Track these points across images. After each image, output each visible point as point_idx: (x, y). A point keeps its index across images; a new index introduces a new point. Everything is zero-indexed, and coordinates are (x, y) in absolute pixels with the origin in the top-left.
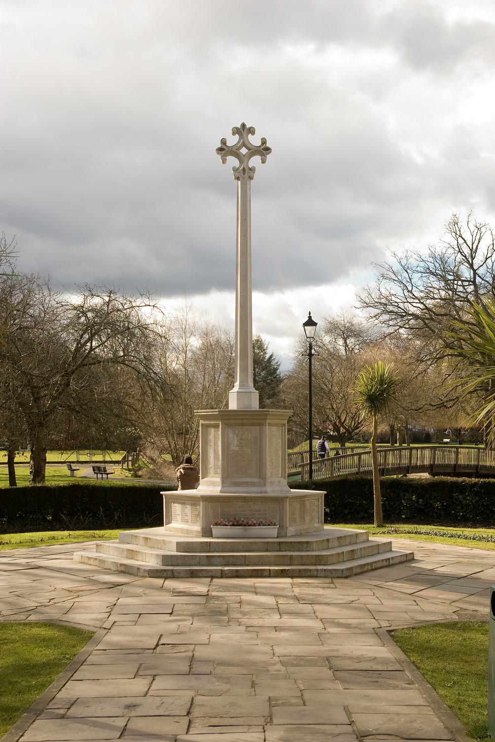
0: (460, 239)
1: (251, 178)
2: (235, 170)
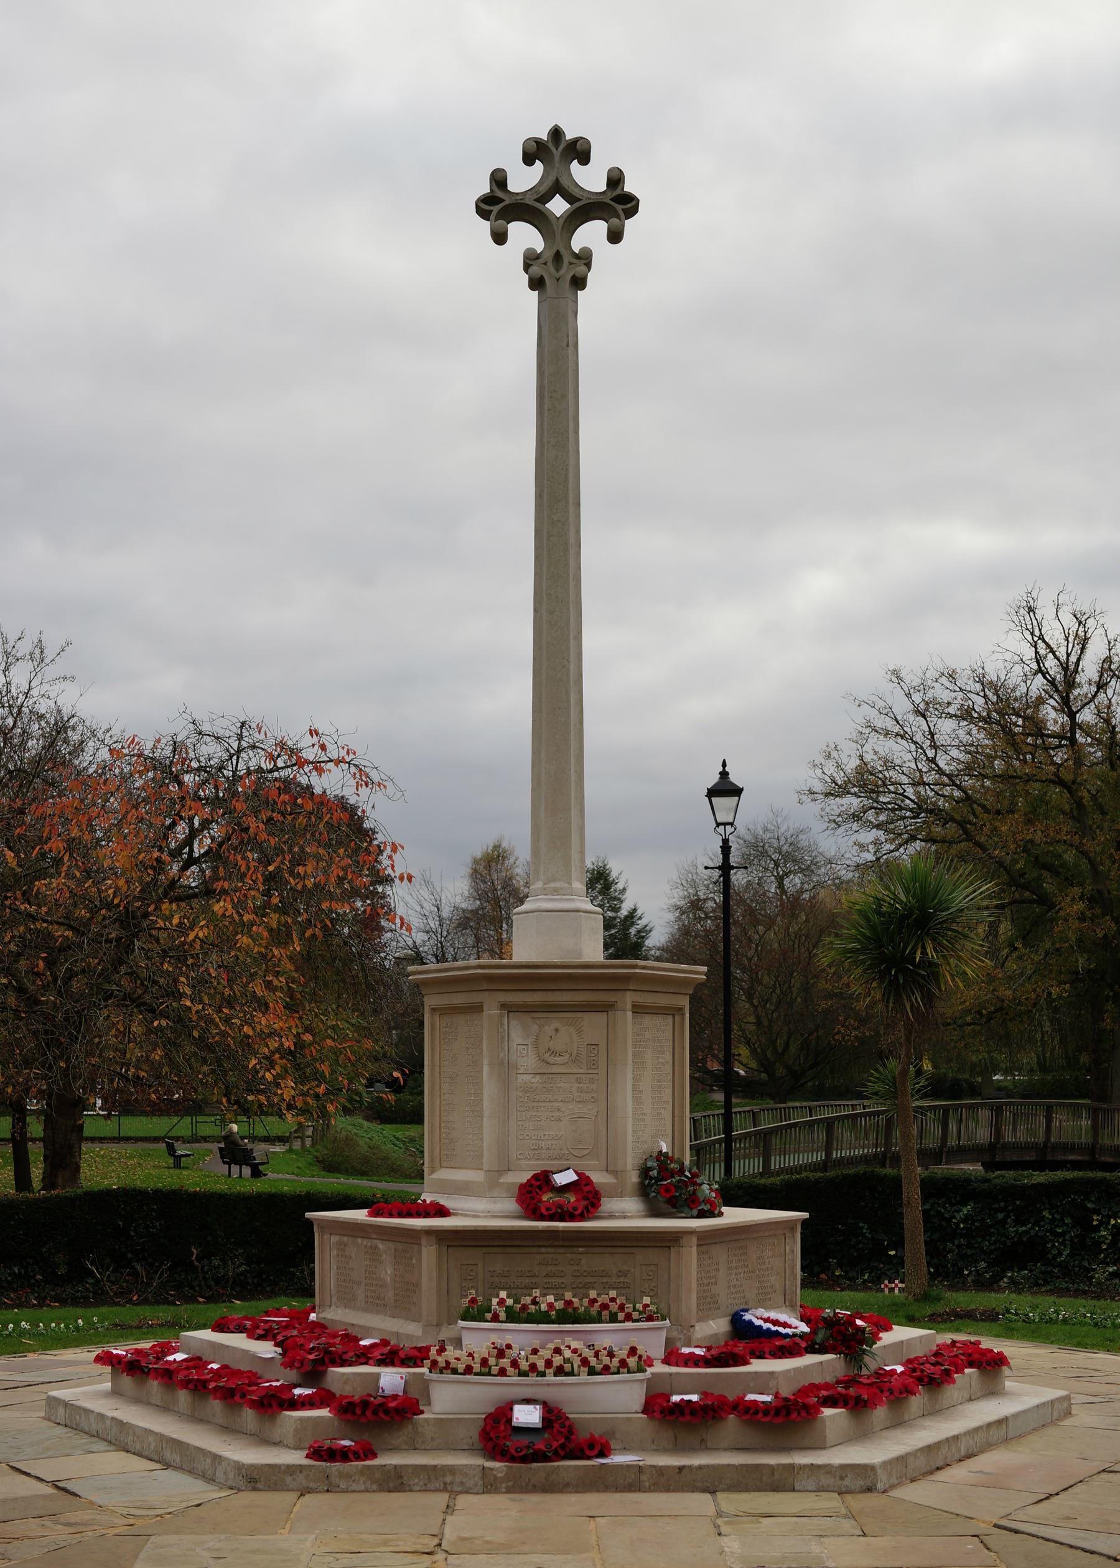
0: (1041, 644)
1: (579, 283)
2: (530, 260)
